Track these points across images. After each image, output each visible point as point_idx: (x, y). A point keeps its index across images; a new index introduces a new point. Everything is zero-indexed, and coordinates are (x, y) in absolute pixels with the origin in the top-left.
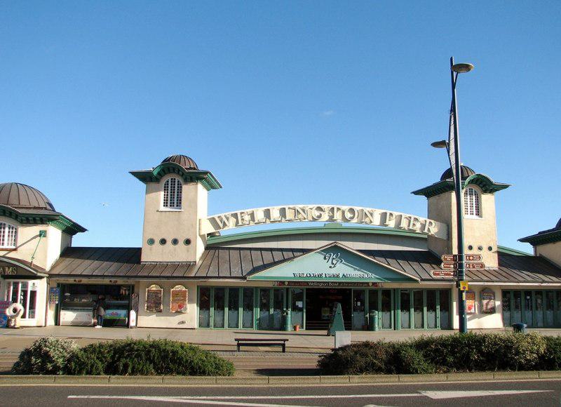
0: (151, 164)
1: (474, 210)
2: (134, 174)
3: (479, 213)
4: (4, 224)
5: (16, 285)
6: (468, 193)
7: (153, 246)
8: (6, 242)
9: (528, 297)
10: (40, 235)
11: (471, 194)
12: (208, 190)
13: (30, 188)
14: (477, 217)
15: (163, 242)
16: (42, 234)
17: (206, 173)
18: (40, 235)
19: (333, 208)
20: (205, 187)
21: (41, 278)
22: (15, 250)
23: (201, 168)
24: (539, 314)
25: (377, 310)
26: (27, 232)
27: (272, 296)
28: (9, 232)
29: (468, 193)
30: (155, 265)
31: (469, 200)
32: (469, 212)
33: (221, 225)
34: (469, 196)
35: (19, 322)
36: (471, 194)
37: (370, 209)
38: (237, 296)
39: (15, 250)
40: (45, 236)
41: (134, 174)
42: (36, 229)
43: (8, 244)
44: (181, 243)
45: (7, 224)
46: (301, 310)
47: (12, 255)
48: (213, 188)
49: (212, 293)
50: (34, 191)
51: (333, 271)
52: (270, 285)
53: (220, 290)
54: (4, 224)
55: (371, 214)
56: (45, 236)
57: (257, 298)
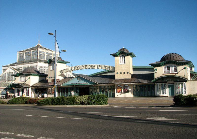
0: (116, 51)
1: (123, 62)
2: (111, 55)
3: (125, 63)
4: (173, 66)
5: (26, 89)
6: (121, 57)
7: (118, 74)
8: (174, 71)
9: (142, 87)
10: (184, 68)
11: (122, 57)
12: (132, 58)
13: (177, 54)
14: (124, 64)
15: (121, 73)
16: (30, 78)
17: (132, 53)
18: (184, 68)
19: (85, 66)
20: (131, 57)
21: (29, 87)
22: (177, 73)
23: (130, 51)
24: (146, 93)
25: (47, 93)
26: (180, 68)
27: (60, 89)
28: (167, 69)
29: (121, 57)
30: (119, 80)
31: (121, 59)
32: (122, 62)
33: (62, 73)
34: (121, 58)
35: (162, 95)
36: (122, 57)
37: (94, 65)
38: (65, 89)
39: (25, 82)
40: (186, 69)
41: (111, 55)
42: (182, 67)
43: (175, 72)
44: (50, 77)
45: (174, 66)
46: (78, 92)
47: (177, 75)
48: (133, 57)
49: (66, 89)
50: (178, 55)
51: (79, 82)
52: (71, 87)
53: (62, 88)
54: (173, 66)
55: (95, 66)
56: (186, 69)
57: (69, 89)
